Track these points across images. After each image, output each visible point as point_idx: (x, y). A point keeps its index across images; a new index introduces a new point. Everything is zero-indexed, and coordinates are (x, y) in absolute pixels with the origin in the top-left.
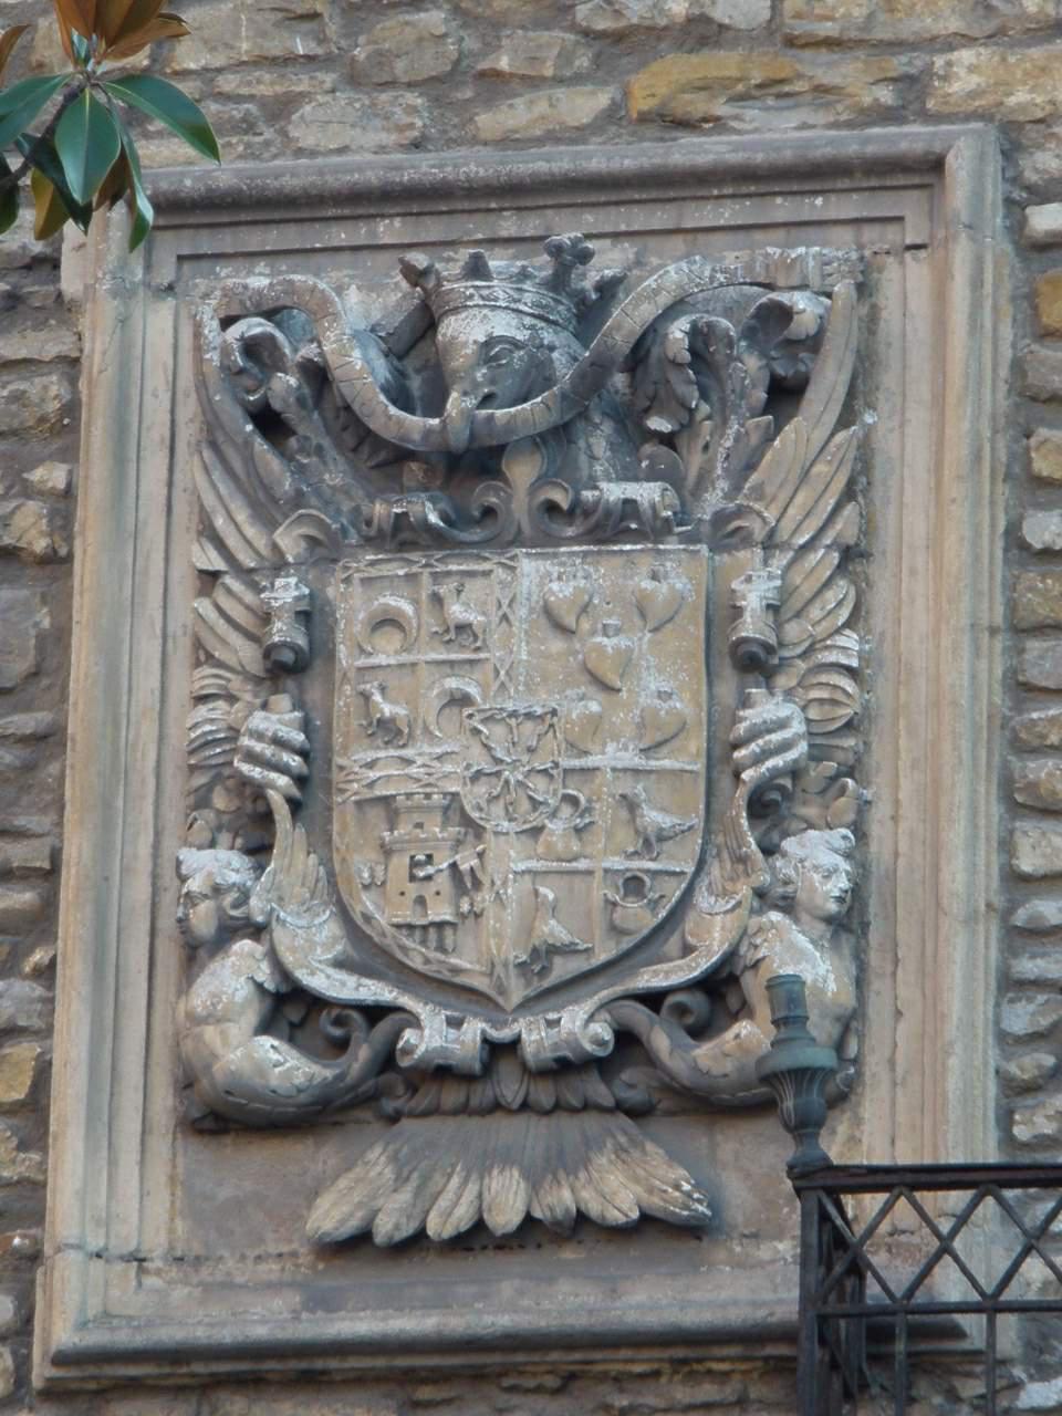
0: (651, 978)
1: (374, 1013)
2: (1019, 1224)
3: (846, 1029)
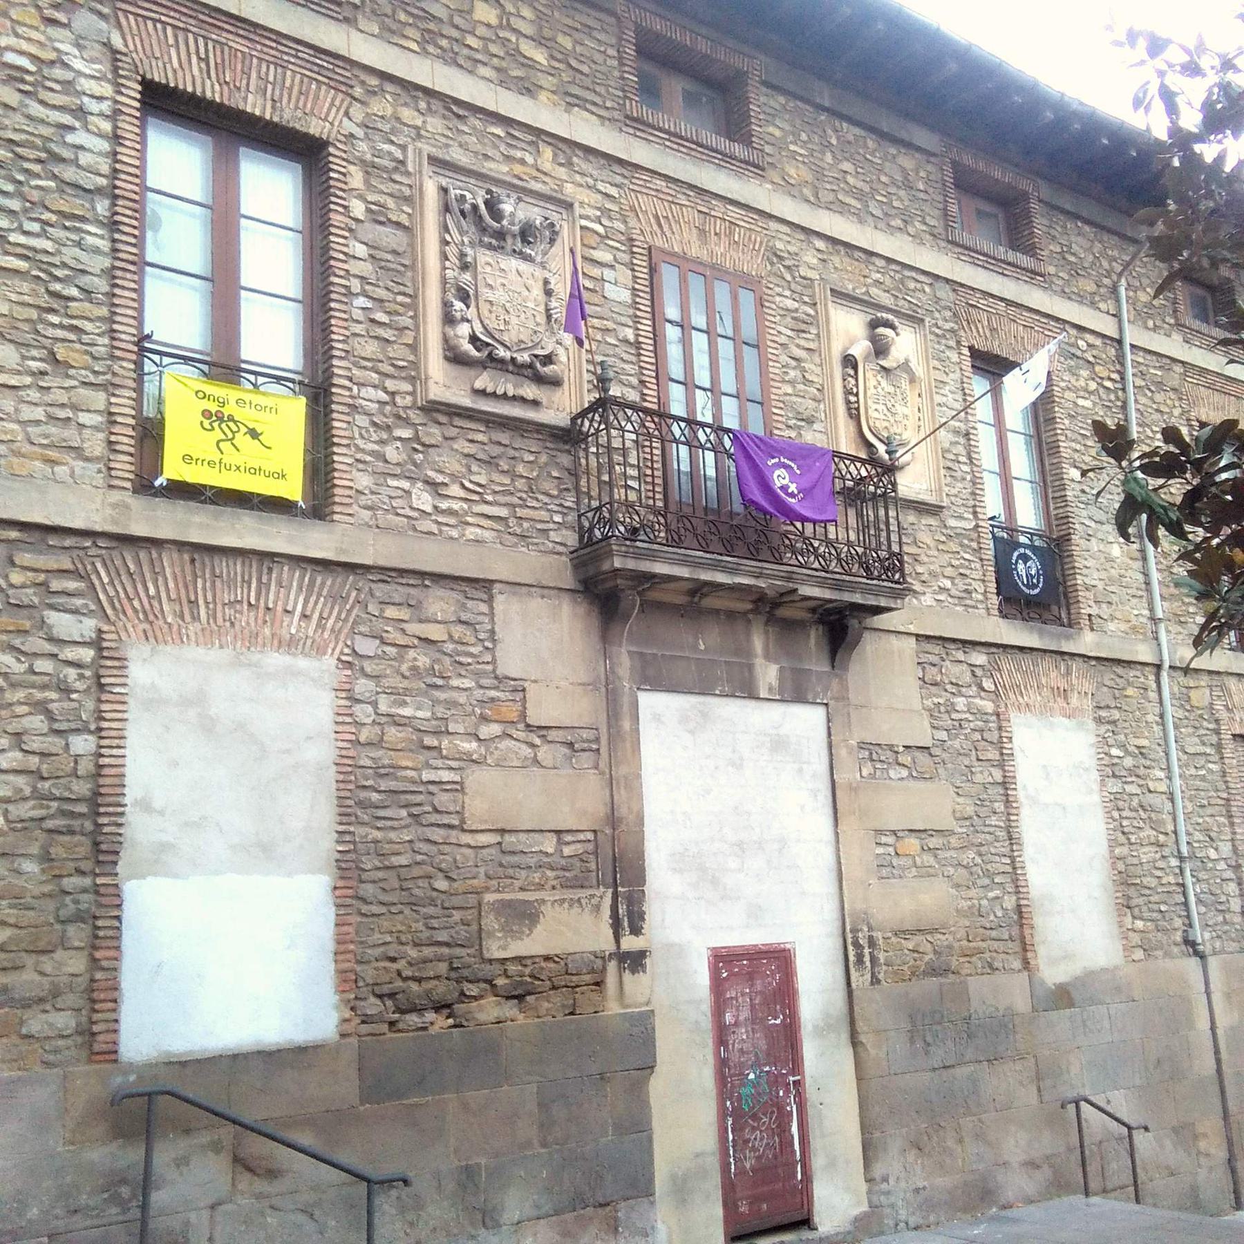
0: (536, 352)
1: (488, 344)
2: (617, 941)
3: (1065, 958)
